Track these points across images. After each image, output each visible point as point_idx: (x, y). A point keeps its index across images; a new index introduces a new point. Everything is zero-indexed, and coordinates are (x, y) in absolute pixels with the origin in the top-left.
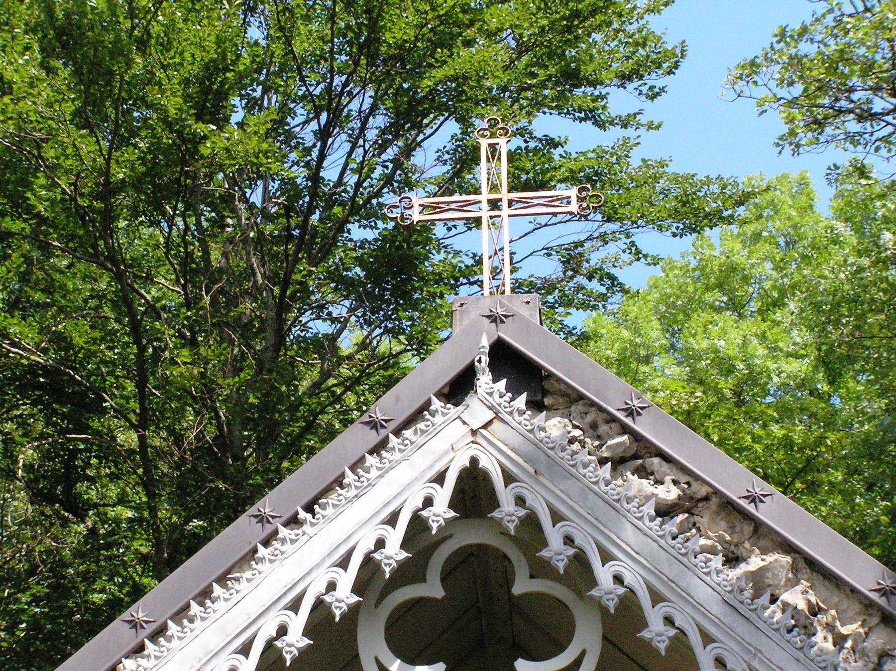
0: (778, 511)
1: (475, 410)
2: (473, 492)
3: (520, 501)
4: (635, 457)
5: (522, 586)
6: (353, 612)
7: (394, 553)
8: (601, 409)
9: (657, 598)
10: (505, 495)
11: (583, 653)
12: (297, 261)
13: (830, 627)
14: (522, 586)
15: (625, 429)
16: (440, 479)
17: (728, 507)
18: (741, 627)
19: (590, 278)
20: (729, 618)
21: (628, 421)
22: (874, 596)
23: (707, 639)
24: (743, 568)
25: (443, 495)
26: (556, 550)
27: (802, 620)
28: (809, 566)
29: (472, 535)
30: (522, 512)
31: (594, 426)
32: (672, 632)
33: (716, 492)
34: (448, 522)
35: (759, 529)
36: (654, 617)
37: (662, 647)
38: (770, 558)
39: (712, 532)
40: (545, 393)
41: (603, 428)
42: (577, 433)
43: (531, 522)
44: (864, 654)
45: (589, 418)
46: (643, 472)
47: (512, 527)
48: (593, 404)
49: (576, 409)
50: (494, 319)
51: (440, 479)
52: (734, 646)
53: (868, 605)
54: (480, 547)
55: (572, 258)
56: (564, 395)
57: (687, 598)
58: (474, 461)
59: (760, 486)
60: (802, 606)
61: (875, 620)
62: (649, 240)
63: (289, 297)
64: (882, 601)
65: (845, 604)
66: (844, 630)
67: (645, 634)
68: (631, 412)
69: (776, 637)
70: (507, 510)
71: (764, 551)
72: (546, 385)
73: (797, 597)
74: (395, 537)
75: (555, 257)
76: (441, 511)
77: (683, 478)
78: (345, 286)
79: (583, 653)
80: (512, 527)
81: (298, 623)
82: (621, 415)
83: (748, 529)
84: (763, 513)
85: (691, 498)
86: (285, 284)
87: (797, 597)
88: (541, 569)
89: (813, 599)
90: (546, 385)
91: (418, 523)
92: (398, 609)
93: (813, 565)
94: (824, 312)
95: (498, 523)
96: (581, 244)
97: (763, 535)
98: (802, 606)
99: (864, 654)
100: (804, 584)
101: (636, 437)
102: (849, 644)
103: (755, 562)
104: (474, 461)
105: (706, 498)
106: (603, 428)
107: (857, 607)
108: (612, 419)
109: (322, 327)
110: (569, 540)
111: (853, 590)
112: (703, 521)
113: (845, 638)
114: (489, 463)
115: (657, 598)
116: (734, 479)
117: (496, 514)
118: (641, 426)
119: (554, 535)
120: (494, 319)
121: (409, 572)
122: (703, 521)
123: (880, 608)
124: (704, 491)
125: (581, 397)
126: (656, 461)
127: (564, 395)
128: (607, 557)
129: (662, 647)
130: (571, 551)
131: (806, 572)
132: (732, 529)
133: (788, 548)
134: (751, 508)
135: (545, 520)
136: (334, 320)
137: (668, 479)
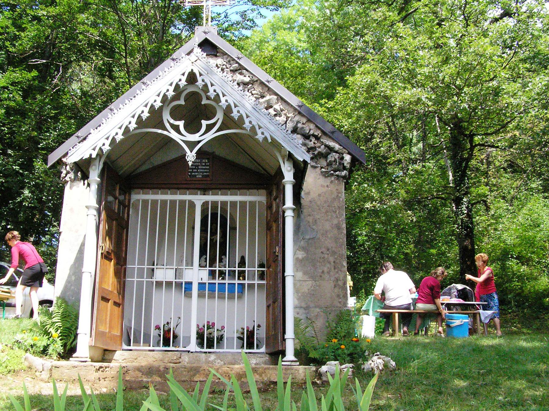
0: (276, 86)
1: (193, 57)
2: (192, 78)
3: (203, 81)
4: (239, 70)
5: (204, 102)
6: (161, 108)
7: (171, 94)
8: (231, 57)
9: (236, 106)
10: (199, 79)
11: (219, 119)
12: (168, 13)
13: (285, 114)
14: (204, 102)
15: (237, 63)
16: (183, 74)
17: (262, 83)
18: (256, 114)
19: (248, 21)
20: (253, 111)
21: (238, 60)
22: (297, 107)
23: (248, 116)
24: (265, 99)
25: (184, 78)
26: (212, 94)
27: (279, 113)
28: (281, 99)
29: (191, 89)
30: (204, 83)
31: (229, 61)
32: (239, 114)
33: (259, 79)
34: (185, 85)
35: (269, 89)
36: (235, 110)
37: (236, 118)
38: (272, 96)
39: (258, 90)
40: (217, 52)
41: (232, 62)
42: (225, 63)
43: (206, 86)
44: (293, 122)
45: (228, 59)
46: (241, 74)
47: (201, 87)
48: (229, 56)
49: (226, 56)
50: (205, 33)
51: (183, 74)
52: (254, 118)
53: (295, 109)
54: (196, 92)
55: (243, 15)
56: (222, 53)
57: (244, 106)
58: (192, 70)
59: (270, 78)
60: (279, 109)
61: (297, 113)
62: (263, 11)
63: (167, 24)
64: (298, 109)
65: (290, 109)
66: (289, 115)
67: (232, 115)
68: (239, 58)
69: (265, 116)
70: (200, 83)
71: (270, 95)
72: (218, 50)
73: (278, 107)
74: (172, 89)
75: (239, 14)
76: (183, 83)
77: (251, 76)
78: (183, 21)
79: (219, 119)
80: (201, 87)
81: (146, 110)
82: (236, 59)
83: (267, 89)
84: (270, 85)
85: (253, 81)
86: (165, 19)
87: (278, 107)
88: (208, 98)
89: (282, 108)
90: (218, 50)
91: (177, 86)
92: (173, 107)
93: (282, 99)
94: (310, 32)
95: (197, 86)
96: (246, 11)
97: (270, 90)
98: (279, 109)
99: (293, 122)
100: (280, 103)
101: (240, 65)
102: (290, 119)
103: (268, 97)
104: (192, 70)
105: (257, 81)
106: (232, 62)
107: (292, 110)
108: (234, 60)
109: (178, 32)
110: (215, 91)
111: (292, 106)
112: (256, 87)
113: (289, 117)
114: (196, 71)
115: (236, 106)
116: (264, 76)
117: (197, 84)
118: (241, 62)
119: (211, 89)
120: (205, 33)
121: (175, 98)
122: (256, 87)
123: (298, 111)
124: (256, 79)
125: (227, 54)
126: (244, 71)
127: (222, 53)
128: (224, 95)
129: (236, 118)
130: (215, 94)
131: (280, 101)
132: (263, 89)
133: (276, 94)
134: (267, 84)
135: (209, 85)
136: (179, 30)
137: (247, 76)
